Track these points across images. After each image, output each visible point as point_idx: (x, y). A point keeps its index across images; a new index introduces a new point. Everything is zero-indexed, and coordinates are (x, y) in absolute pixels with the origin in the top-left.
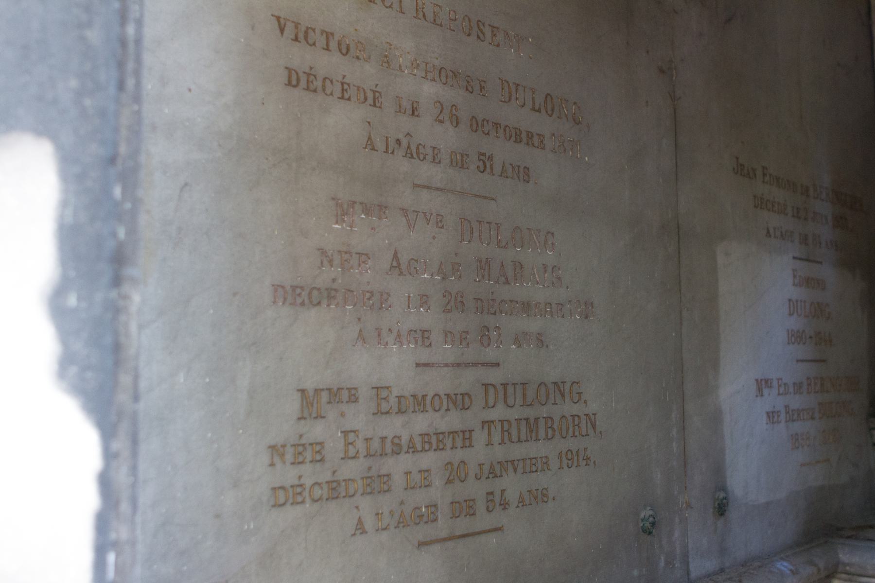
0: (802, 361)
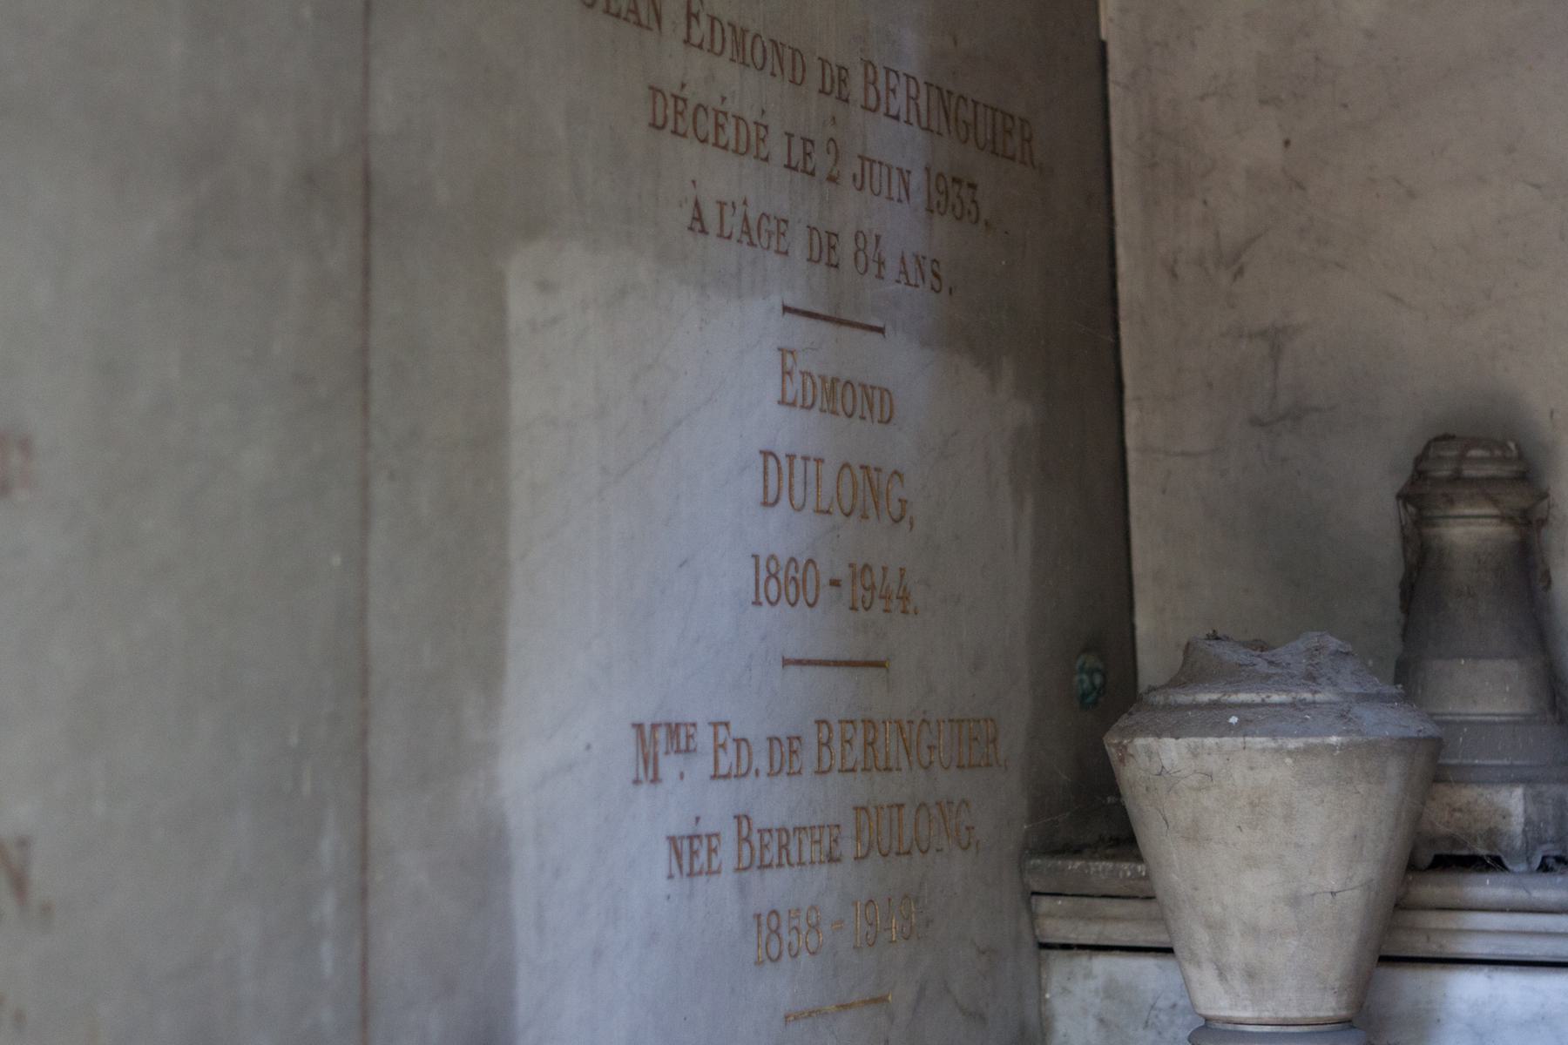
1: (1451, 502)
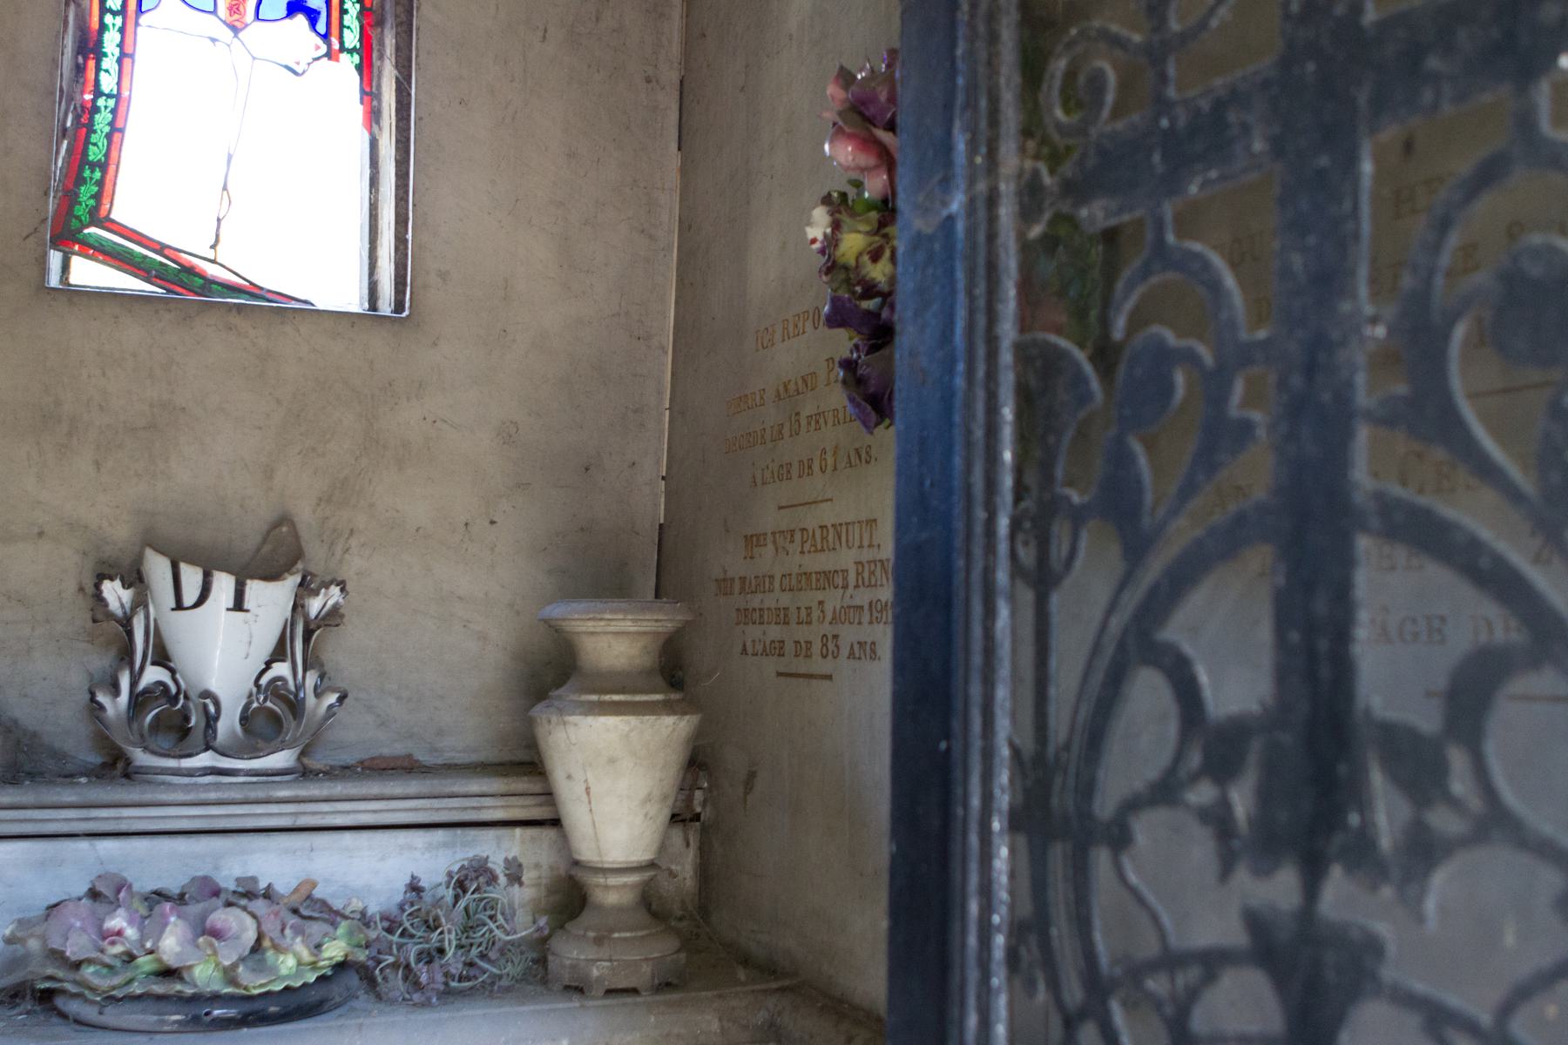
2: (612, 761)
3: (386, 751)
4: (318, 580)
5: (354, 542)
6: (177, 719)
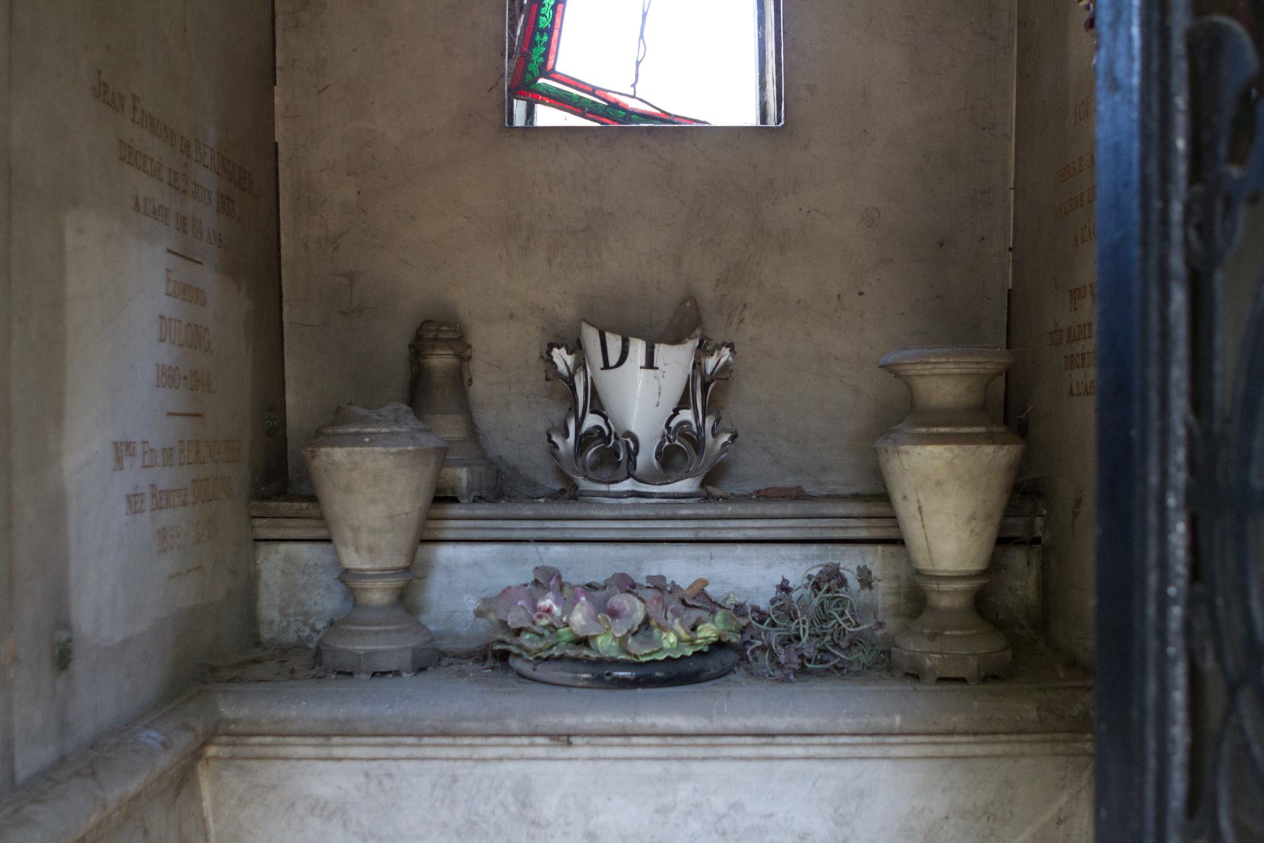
0: (173, 414)
1: (434, 348)
2: (939, 484)
3: (780, 484)
4: (713, 343)
5: (747, 314)
6: (610, 452)
